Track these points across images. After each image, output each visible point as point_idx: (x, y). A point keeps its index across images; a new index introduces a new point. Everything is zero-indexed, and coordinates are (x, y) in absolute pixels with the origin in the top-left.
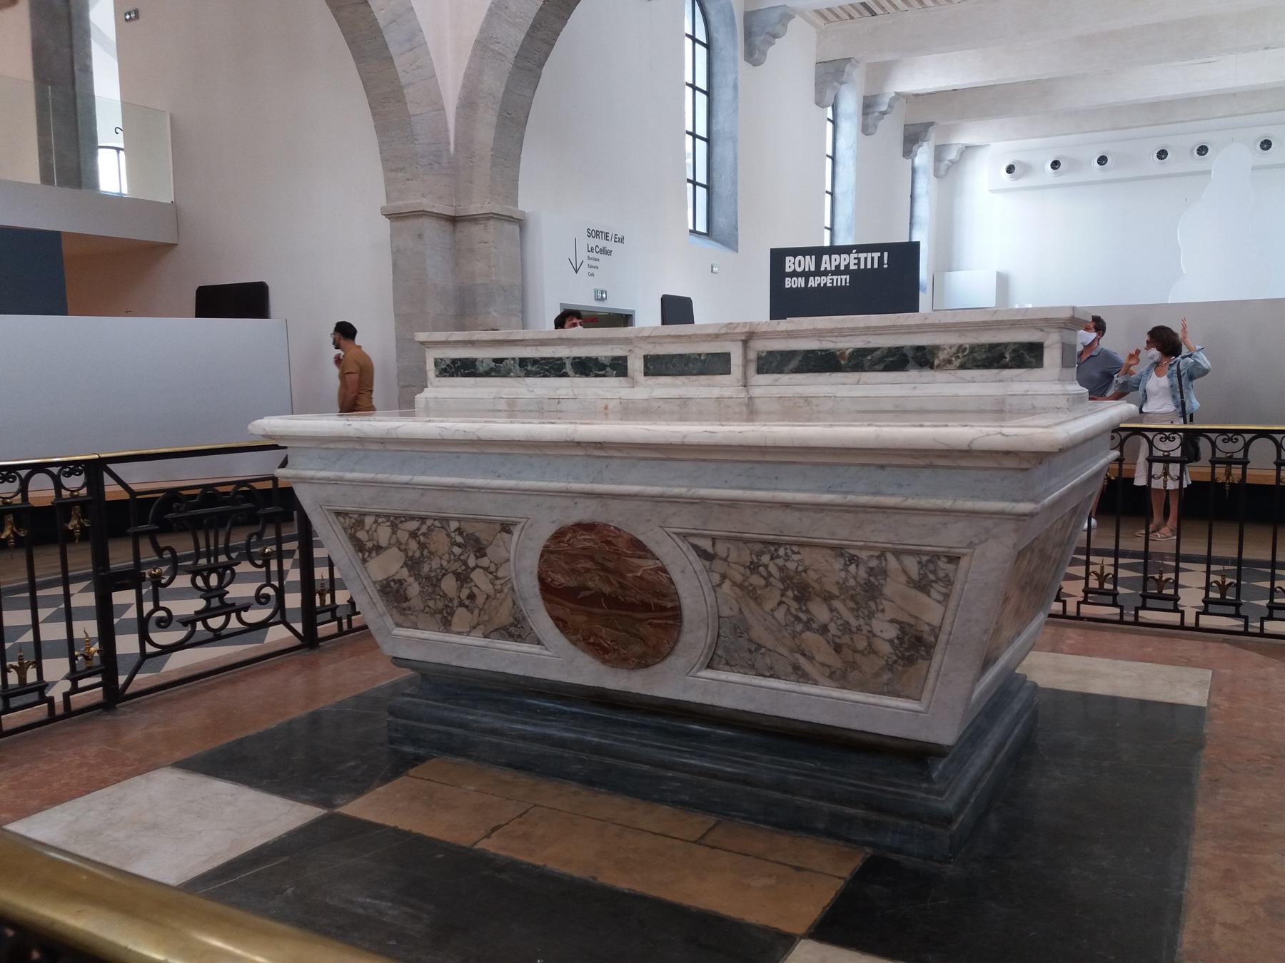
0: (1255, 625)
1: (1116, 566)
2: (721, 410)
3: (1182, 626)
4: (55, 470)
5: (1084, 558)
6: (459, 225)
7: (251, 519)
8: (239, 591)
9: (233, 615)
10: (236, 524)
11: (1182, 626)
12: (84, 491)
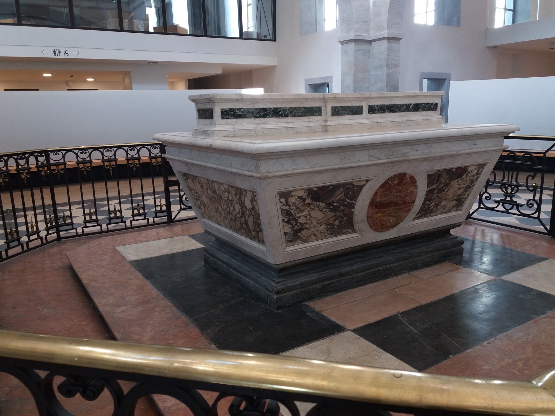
0: (80, 230)
1: (120, 203)
2: (312, 132)
3: (126, 228)
4: (76, 151)
5: (106, 202)
6: (373, 43)
7: (529, 169)
8: (522, 198)
9: (515, 207)
10: (523, 170)
11: (126, 228)
12: (45, 162)
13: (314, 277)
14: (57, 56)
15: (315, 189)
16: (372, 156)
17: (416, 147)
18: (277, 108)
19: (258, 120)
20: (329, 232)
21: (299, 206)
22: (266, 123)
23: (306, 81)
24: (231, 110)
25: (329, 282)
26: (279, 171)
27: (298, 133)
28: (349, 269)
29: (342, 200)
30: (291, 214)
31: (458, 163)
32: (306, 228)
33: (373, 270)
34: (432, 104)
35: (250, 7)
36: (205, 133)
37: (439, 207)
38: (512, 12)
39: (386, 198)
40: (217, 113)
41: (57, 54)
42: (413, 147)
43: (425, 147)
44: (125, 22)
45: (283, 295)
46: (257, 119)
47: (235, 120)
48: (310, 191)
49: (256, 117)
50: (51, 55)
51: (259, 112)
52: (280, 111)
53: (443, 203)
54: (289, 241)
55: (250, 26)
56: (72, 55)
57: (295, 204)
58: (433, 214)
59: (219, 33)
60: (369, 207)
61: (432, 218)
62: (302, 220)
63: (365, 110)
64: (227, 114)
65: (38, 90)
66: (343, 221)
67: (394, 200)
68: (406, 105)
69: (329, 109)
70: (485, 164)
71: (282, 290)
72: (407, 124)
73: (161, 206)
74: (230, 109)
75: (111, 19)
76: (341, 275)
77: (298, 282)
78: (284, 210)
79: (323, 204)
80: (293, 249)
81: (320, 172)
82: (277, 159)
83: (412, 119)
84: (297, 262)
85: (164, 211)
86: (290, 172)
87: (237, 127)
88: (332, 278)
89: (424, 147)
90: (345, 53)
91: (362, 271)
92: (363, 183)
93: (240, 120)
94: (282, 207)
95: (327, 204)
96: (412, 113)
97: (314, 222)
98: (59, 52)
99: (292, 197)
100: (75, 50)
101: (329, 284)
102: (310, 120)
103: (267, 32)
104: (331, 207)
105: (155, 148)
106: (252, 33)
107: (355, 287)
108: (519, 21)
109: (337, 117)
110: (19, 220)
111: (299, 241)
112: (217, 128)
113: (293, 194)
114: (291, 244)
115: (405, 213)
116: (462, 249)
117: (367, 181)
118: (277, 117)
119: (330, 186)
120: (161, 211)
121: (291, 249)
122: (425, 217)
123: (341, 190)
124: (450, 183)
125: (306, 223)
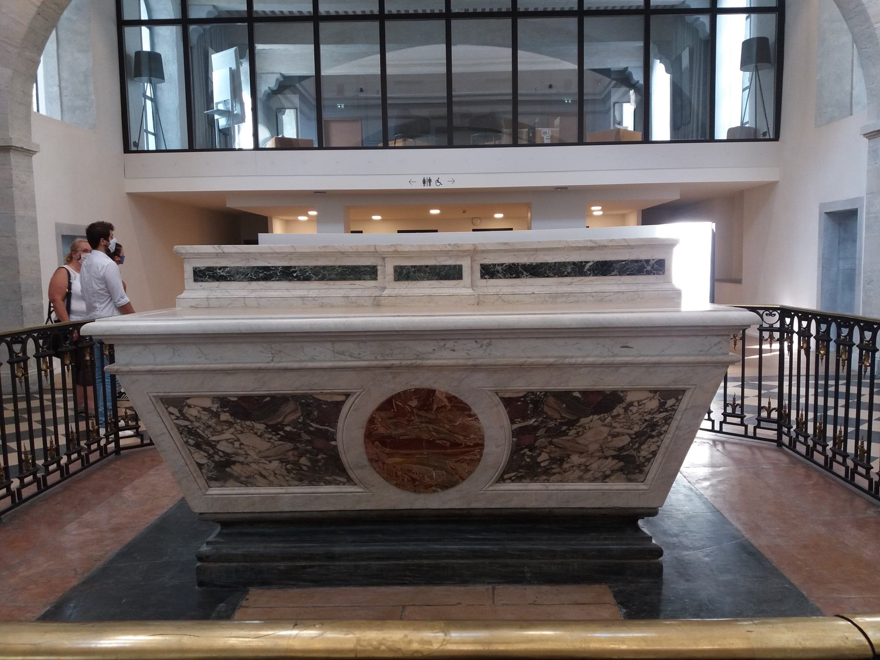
2: (353, 305)
13: (275, 547)
14: (427, 187)
15: (233, 399)
16: (343, 353)
17: (450, 344)
18: (291, 267)
19: (255, 285)
20: (292, 475)
21: (210, 423)
22: (270, 289)
23: (822, 205)
24: (209, 269)
25: (303, 564)
26: (141, 365)
27: (324, 306)
28: (351, 548)
29: (300, 423)
30: (197, 435)
31: (609, 383)
32: (239, 462)
33: (409, 561)
34: (647, 261)
37: (566, 466)
39: (401, 431)
41: (427, 183)
42: (442, 343)
43: (474, 345)
45: (211, 565)
46: (254, 284)
47: (216, 284)
48: (223, 401)
49: (252, 280)
50: (419, 186)
51: (256, 272)
52: (295, 272)
53: (575, 459)
54: (210, 479)
56: (446, 185)
57: (200, 418)
58: (552, 478)
59: (708, 135)
60: (365, 443)
61: (552, 486)
62: (223, 447)
65: (436, 231)
66: (317, 461)
67: (425, 436)
68: (574, 263)
69: (390, 270)
70: (683, 391)
71: (207, 557)
72: (571, 299)
73: (769, 411)
74: (208, 268)
76: (331, 557)
77: (239, 551)
78: (181, 426)
79: (260, 427)
80: (221, 492)
81: (235, 371)
82: (144, 345)
83: (588, 289)
84: (239, 516)
85: (773, 421)
86: (159, 367)
88: (311, 557)
89: (471, 344)
91: (378, 559)
92: (340, 398)
93: (223, 284)
94: (176, 421)
95: (268, 426)
96: (591, 278)
97: (253, 455)
98: (430, 181)
99: (190, 406)
101: (304, 567)
102: (353, 286)
104: (281, 433)
105: (771, 314)
107: (362, 585)
109: (406, 282)
110: (57, 396)
111: (231, 481)
113: (189, 401)
114: (217, 484)
115: (465, 465)
116: (660, 568)
117: (347, 395)
118: (290, 280)
119: (265, 396)
120: (769, 420)
121: (217, 492)
122: (532, 480)
123: (291, 405)
124: (578, 420)
125: (237, 454)
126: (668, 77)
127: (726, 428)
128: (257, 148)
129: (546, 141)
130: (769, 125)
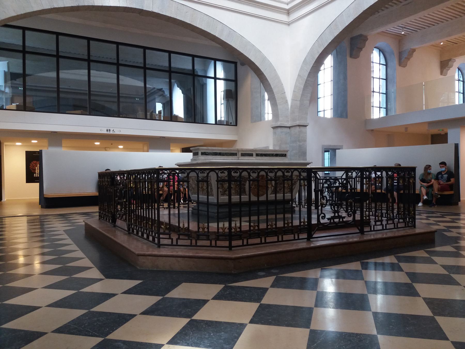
14: (108, 133)
19: (213, 156)
35: (223, 105)
36: (195, 160)
38: (385, 109)
40: (200, 153)
44: (148, 114)
50: (105, 132)
55: (222, 115)
56: (117, 132)
63: (254, 155)
64: (203, 154)
69: (240, 154)
75: (140, 112)
87: (206, 158)
90: (275, 133)
93: (207, 156)
98: (110, 130)
100: (119, 130)
103: (232, 120)
106: (223, 121)
108: (390, 114)
112: (200, 158)
126: (182, 95)
127: (180, 242)
128: (216, 124)
129: (157, 119)
130: (233, 119)
